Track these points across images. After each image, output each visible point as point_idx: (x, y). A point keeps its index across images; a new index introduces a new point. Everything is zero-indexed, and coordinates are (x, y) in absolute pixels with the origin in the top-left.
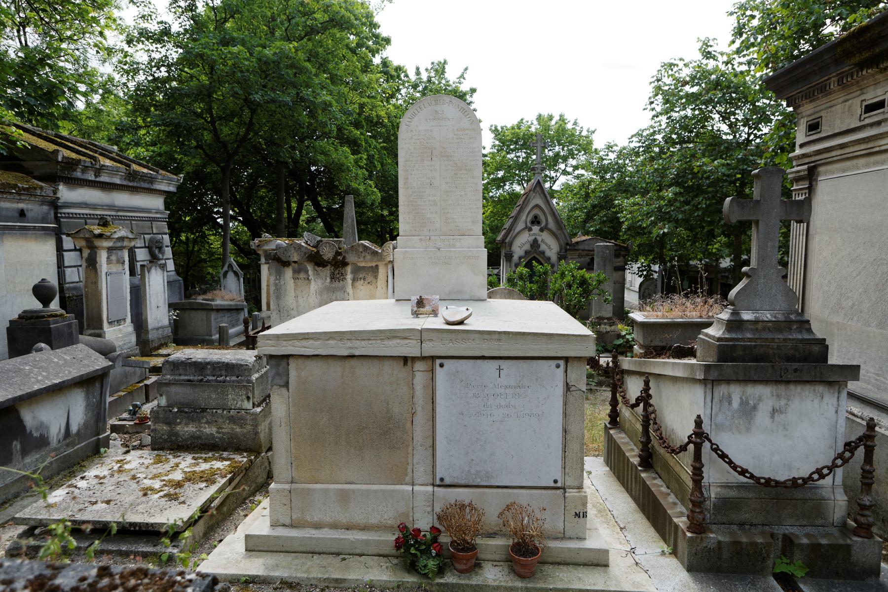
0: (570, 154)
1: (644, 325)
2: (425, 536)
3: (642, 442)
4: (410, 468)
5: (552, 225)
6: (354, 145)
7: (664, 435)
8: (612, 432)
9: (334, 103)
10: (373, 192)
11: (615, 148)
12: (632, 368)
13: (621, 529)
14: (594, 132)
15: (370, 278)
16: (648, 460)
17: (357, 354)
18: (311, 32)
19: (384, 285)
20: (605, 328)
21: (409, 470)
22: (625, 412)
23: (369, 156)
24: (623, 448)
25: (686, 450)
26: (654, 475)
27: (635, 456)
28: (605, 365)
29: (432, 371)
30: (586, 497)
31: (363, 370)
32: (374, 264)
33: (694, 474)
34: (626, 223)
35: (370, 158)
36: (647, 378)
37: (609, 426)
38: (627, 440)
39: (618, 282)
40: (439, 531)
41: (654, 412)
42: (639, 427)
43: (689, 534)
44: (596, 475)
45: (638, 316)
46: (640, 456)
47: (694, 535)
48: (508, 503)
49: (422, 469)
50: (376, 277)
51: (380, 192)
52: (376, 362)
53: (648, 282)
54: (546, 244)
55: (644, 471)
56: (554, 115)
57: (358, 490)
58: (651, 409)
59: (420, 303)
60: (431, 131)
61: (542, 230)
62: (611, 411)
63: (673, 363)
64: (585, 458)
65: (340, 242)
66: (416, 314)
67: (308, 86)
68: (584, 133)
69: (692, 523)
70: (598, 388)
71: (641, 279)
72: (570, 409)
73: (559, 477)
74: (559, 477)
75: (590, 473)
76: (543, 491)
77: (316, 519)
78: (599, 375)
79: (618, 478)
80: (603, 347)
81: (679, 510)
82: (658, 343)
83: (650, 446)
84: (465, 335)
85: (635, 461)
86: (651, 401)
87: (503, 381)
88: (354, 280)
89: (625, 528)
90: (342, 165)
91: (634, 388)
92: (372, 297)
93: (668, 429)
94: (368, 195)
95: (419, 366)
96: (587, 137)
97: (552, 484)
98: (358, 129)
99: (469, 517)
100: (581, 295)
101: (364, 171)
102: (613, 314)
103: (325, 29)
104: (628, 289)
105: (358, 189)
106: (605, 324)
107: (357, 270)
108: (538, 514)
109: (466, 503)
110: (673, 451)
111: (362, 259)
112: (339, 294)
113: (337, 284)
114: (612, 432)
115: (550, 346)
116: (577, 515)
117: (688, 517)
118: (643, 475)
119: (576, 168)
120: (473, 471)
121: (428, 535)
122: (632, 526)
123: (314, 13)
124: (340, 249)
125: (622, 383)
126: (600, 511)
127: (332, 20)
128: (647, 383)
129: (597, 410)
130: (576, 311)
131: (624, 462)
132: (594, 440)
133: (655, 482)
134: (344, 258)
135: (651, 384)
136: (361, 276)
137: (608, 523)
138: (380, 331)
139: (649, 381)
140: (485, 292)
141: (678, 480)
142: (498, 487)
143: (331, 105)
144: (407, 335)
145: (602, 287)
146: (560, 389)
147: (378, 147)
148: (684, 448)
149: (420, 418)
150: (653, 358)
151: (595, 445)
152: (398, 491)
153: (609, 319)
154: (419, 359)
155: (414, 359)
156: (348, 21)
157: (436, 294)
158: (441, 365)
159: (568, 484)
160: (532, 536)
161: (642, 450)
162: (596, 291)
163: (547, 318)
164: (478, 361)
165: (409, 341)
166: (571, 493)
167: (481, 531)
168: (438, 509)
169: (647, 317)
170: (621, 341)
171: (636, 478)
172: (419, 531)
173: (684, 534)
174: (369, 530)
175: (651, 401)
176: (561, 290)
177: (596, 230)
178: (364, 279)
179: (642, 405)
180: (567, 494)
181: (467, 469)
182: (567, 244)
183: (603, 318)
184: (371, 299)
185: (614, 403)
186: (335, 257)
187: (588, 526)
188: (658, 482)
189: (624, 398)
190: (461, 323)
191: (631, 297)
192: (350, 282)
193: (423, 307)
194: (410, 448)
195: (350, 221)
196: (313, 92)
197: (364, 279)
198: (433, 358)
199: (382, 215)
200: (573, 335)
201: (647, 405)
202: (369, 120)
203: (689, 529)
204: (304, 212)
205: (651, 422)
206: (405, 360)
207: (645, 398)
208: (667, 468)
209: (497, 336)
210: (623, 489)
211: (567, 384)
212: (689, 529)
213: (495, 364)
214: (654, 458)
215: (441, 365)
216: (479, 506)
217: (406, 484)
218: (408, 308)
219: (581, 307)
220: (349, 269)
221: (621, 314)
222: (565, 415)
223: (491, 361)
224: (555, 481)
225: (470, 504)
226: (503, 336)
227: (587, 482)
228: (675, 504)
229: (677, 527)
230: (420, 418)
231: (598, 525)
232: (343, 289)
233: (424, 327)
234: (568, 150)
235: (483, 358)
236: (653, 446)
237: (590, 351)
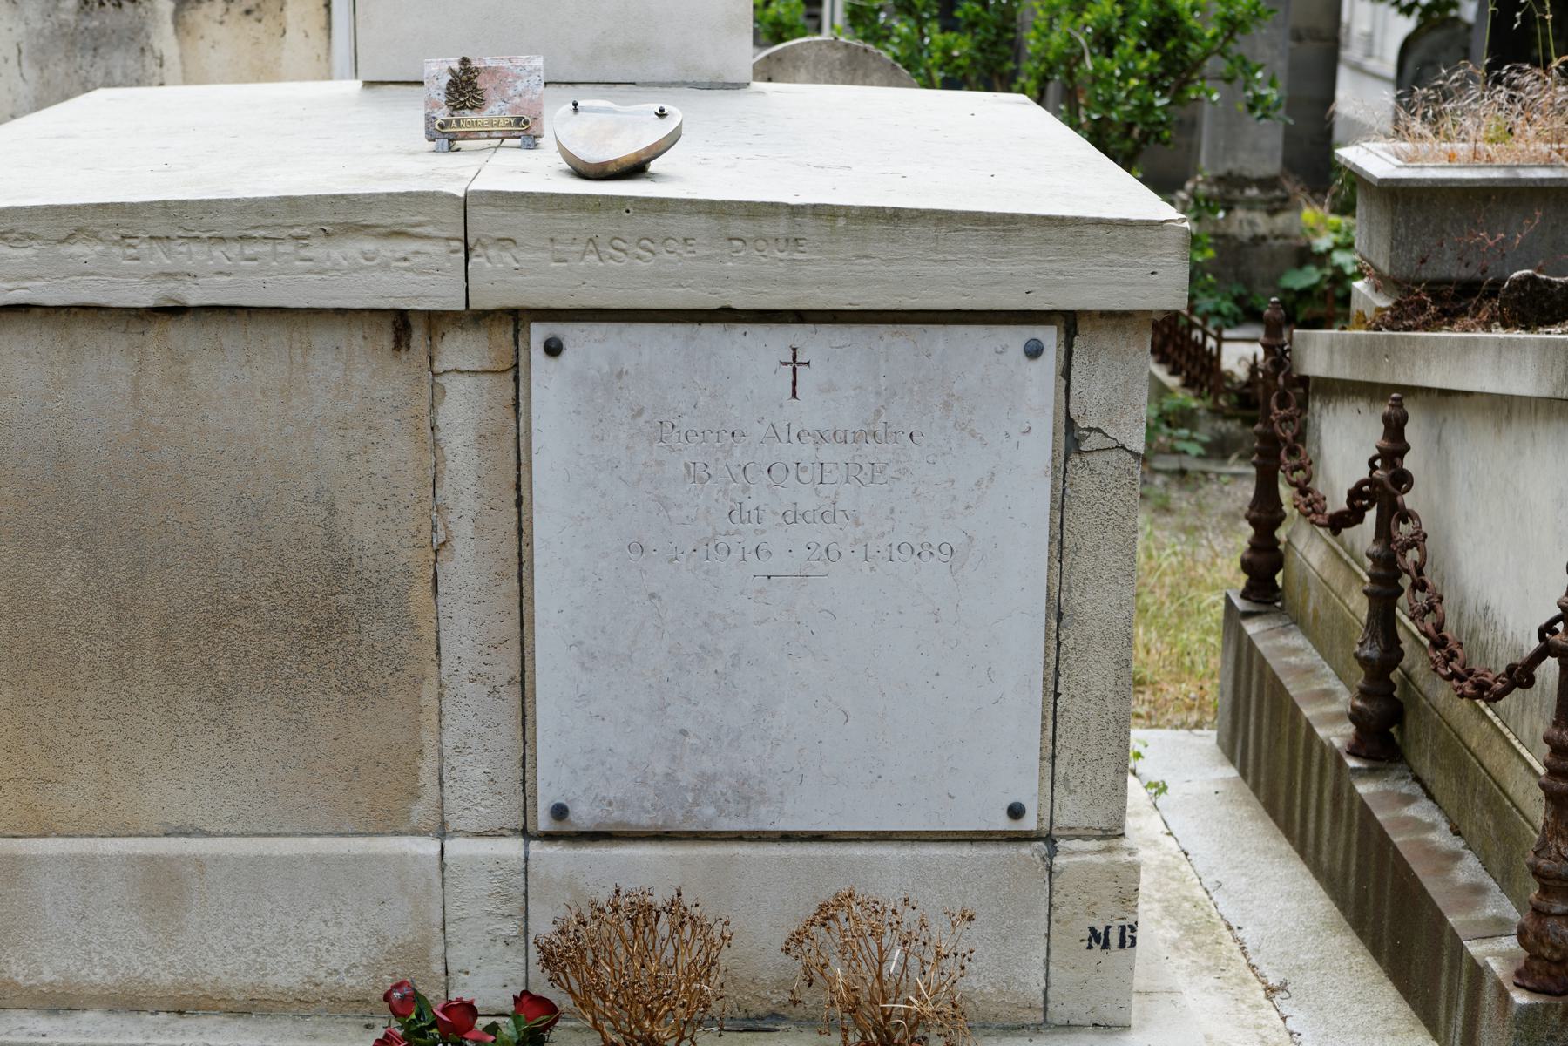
1: (1399, 197)
2: (493, 1029)
3: (1364, 662)
4: (428, 767)
7: (1450, 630)
8: (1252, 628)
12: (1343, 370)
13: (1270, 991)
16: (1384, 732)
17: (192, 302)
20: (1248, 222)
21: (428, 779)
22: (1308, 549)
24: (1294, 689)
25: (1530, 682)
26: (1407, 787)
27: (1335, 719)
28: (1242, 373)
29: (516, 371)
30: (1135, 868)
31: (222, 369)
33: (1553, 772)
36: (1396, 406)
37: (1240, 605)
38: (1311, 656)
39: (1315, 34)
40: (549, 1007)
41: (1418, 540)
42: (1359, 605)
43: (1520, 998)
44: (1182, 801)
45: (1373, 158)
46: (1356, 716)
47: (1540, 1000)
48: (827, 896)
49: (478, 772)
52: (277, 336)
53: (1437, 37)
55: (1371, 773)
57: (218, 860)
58: (1405, 530)
59: (464, 88)
62: (1254, 547)
63: (1500, 342)
64: (1137, 735)
66: (446, 137)
69: (1534, 957)
70: (1212, 466)
71: (1407, 25)
72: (1080, 522)
73: (1029, 793)
74: (1029, 793)
75: (1161, 788)
76: (966, 851)
77: (48, 976)
78: (1216, 412)
79: (1271, 807)
80: (1238, 300)
81: (1490, 911)
82: (1449, 268)
83: (1396, 675)
84: (648, 222)
85: (1338, 735)
86: (1409, 500)
87: (811, 411)
89: (1283, 987)
91: (1344, 449)
92: (265, 72)
93: (1469, 608)
95: (459, 351)
97: (1004, 823)
99: (669, 952)
100: (1153, 82)
102: (1289, 164)
104: (1358, 68)
106: (1251, 205)
108: (941, 932)
109: (659, 899)
110: (1482, 689)
112: (119, 60)
114: (1252, 628)
115: (1005, 268)
116: (1098, 938)
117: (1522, 935)
118: (1364, 788)
120: (686, 778)
121: (508, 1028)
122: (1312, 979)
125: (1301, 436)
126: (1190, 930)
128: (1395, 428)
129: (1203, 554)
130: (1124, 142)
131: (1293, 743)
132: (1182, 668)
133: (1411, 811)
135: (1411, 433)
137: (1218, 970)
138: (292, 204)
139: (1405, 418)
140: (743, 54)
141: (1496, 799)
142: (787, 837)
144: (405, 218)
145: (1241, 46)
146: (1039, 446)
148: (1521, 675)
149: (469, 565)
150: (1426, 326)
151: (1189, 688)
152: (381, 859)
153: (1266, 183)
154: (461, 324)
155: (437, 321)
157: (533, 51)
158: (553, 349)
159: (1063, 820)
160: (921, 1019)
161: (1364, 694)
162: (1213, 65)
163: (1012, 156)
164: (707, 330)
165: (411, 246)
166: (1076, 856)
167: (716, 1007)
168: (543, 927)
169: (1410, 160)
170: (1309, 277)
171: (1336, 804)
172: (469, 1009)
173: (1504, 995)
174: (267, 1013)
175: (1409, 500)
176: (1071, 60)
179: (1371, 516)
180: (1060, 861)
181: (660, 767)
183: (1243, 182)
184: (258, 79)
185: (1265, 514)
187: (1139, 982)
188: (1422, 811)
189: (1304, 492)
190: (635, 169)
191: (1362, 98)
193: (478, 103)
194: (429, 691)
198: (517, 318)
200: (1098, 222)
201: (1393, 513)
203: (1524, 978)
205: (1406, 581)
206: (400, 325)
207: (1385, 489)
208: (1458, 757)
209: (782, 227)
210: (1286, 847)
211: (1070, 423)
212: (1524, 978)
213: (779, 339)
214: (1410, 720)
215: (553, 349)
216: (708, 911)
217: (416, 832)
218: (408, 117)
219: (1152, 134)
221: (1314, 163)
222: (1059, 548)
223: (759, 330)
224: (1016, 812)
225: (674, 906)
226: (809, 226)
227: (1142, 822)
228: (1478, 890)
229: (1478, 972)
230: (469, 565)
231: (1180, 981)
232: (136, 40)
233: (480, 185)
235: (726, 315)
236: (1408, 677)
237: (1164, 287)
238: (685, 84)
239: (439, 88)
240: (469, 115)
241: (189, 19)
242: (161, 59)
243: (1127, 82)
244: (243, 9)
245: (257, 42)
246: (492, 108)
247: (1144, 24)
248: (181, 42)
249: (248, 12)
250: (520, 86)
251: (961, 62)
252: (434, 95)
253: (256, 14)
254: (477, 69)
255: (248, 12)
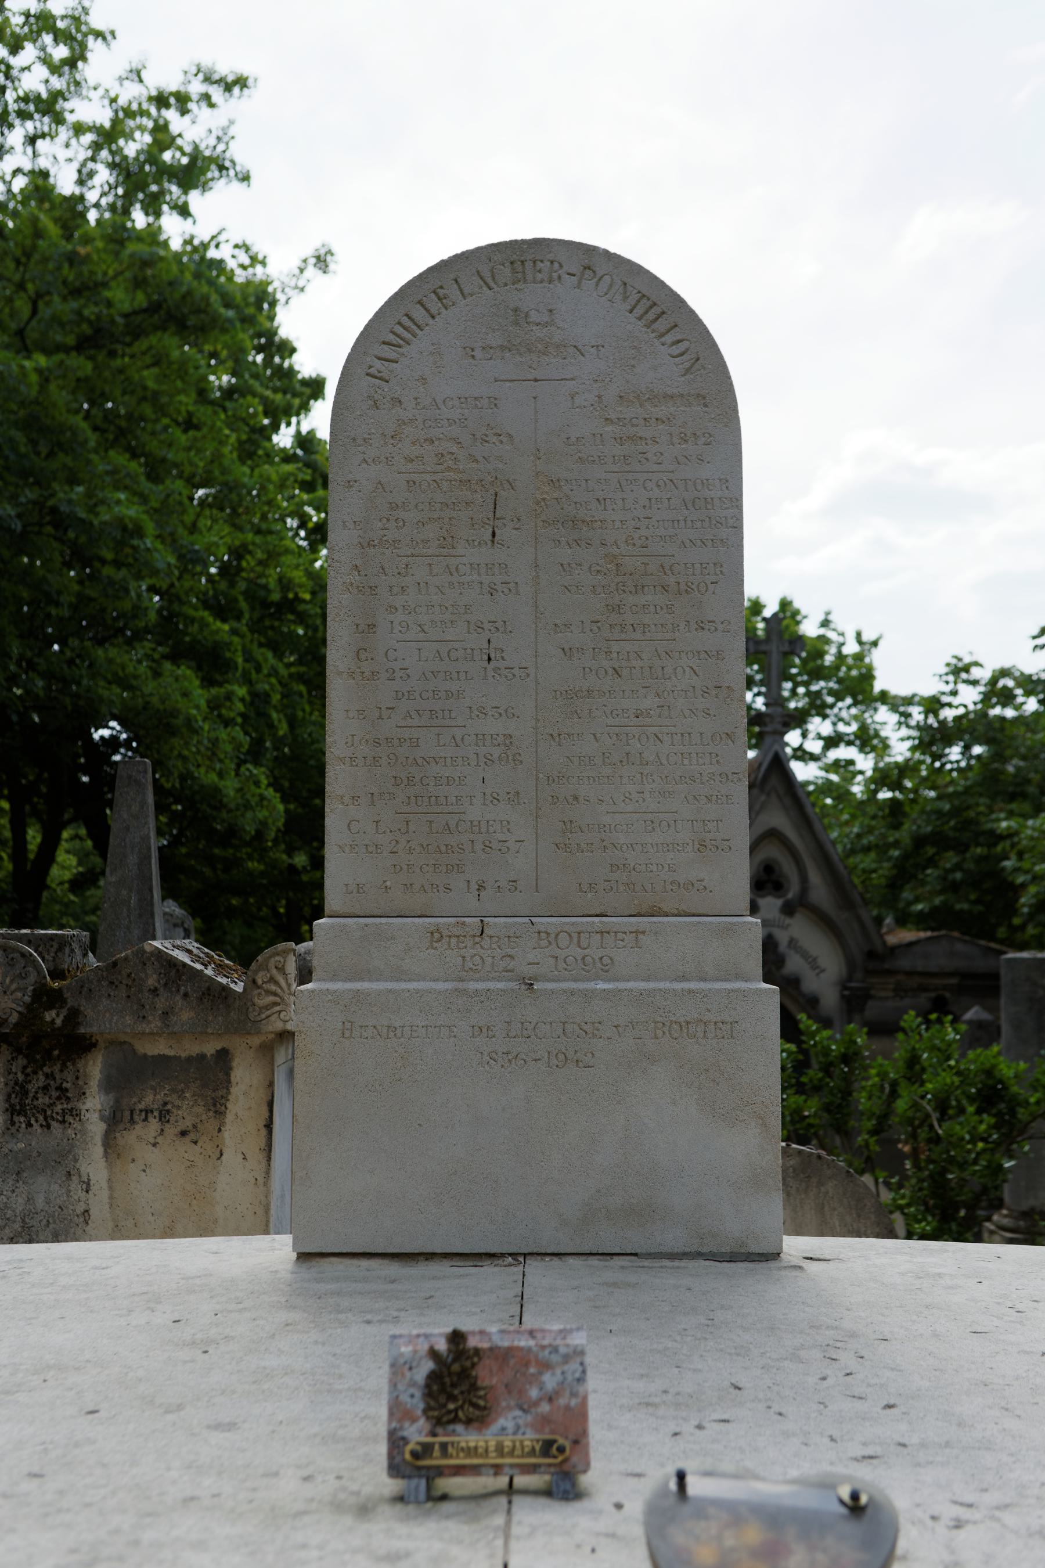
0: (812, 704)
5: (820, 892)
6: (212, 664)
9: (150, 528)
10: (262, 798)
11: (976, 673)
14: (875, 644)
15: (187, 1113)
18: (95, 339)
19: (255, 1143)
23: (254, 695)
32: (210, 1048)
34: (1033, 889)
35: (258, 700)
50: (218, 1107)
51: (284, 800)
54: (805, 955)
56: (763, 600)
60: (494, 402)
61: (788, 910)
65: (63, 943)
67: (73, 481)
68: (851, 648)
88: (117, 1120)
90: (174, 713)
94: (247, 806)
96: (859, 657)
98: (224, 620)
101: (238, 732)
103: (136, 333)
105: (217, 790)
107: (131, 1074)
111: (155, 1024)
113: (35, 1139)
119: (832, 742)
123: (105, 285)
124: (57, 974)
127: (154, 308)
134: (74, 1016)
136: (149, 1099)
143: (139, 531)
147: (283, 672)
156: (202, 308)
177: (934, 911)
178: (164, 1116)
182: (871, 955)
186: (31, 1014)
192: (96, 1127)
193: (479, 1416)
195: (133, 859)
196: (89, 495)
197: (164, 1116)
199: (292, 868)
202: (256, 596)
204: (61, 856)
220: (95, 1068)
232: (63, 1163)
234: (808, 694)
238: (698, 1255)
239: (413, 1384)
240: (467, 1437)
241: (121, 1142)
242: (88, 1184)
243: (975, 1145)
244: (179, 1129)
245: (192, 1165)
246: (501, 1422)
247: (973, 1090)
248: (110, 1165)
249: (183, 1133)
250: (550, 1381)
251: (811, 1121)
252: (405, 1398)
253: (192, 1136)
254: (477, 1351)
255: (183, 1133)
